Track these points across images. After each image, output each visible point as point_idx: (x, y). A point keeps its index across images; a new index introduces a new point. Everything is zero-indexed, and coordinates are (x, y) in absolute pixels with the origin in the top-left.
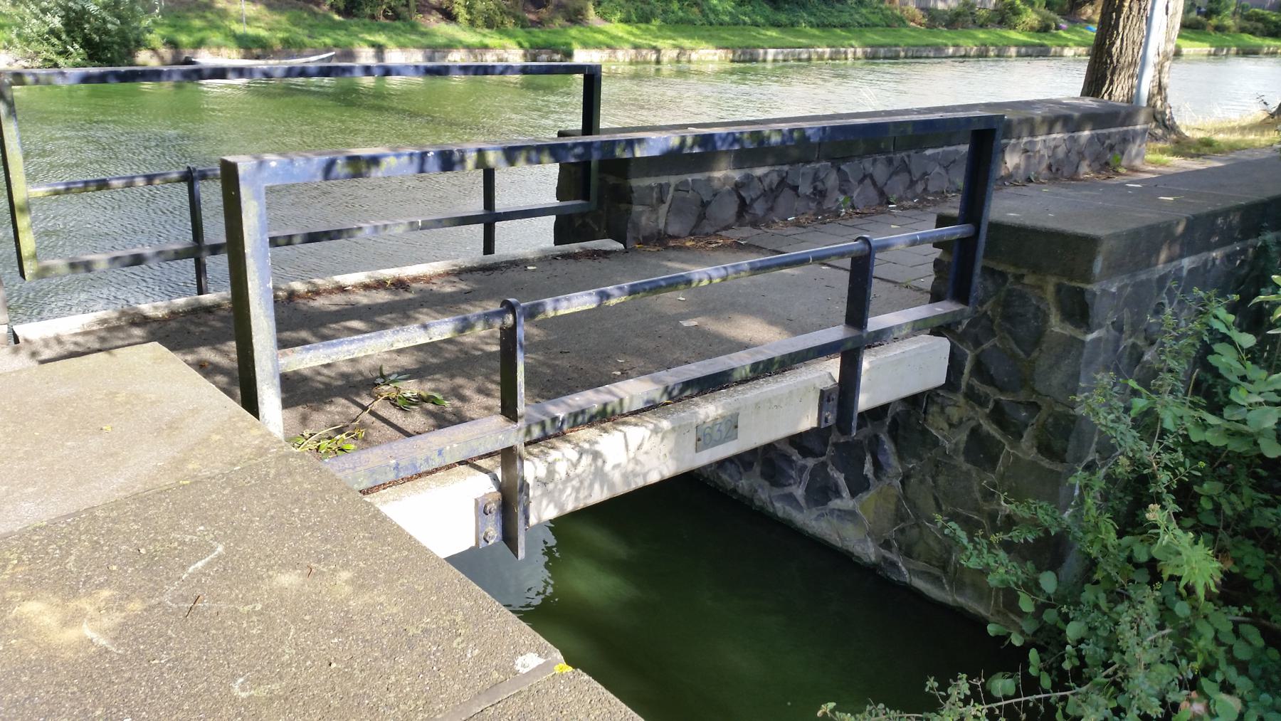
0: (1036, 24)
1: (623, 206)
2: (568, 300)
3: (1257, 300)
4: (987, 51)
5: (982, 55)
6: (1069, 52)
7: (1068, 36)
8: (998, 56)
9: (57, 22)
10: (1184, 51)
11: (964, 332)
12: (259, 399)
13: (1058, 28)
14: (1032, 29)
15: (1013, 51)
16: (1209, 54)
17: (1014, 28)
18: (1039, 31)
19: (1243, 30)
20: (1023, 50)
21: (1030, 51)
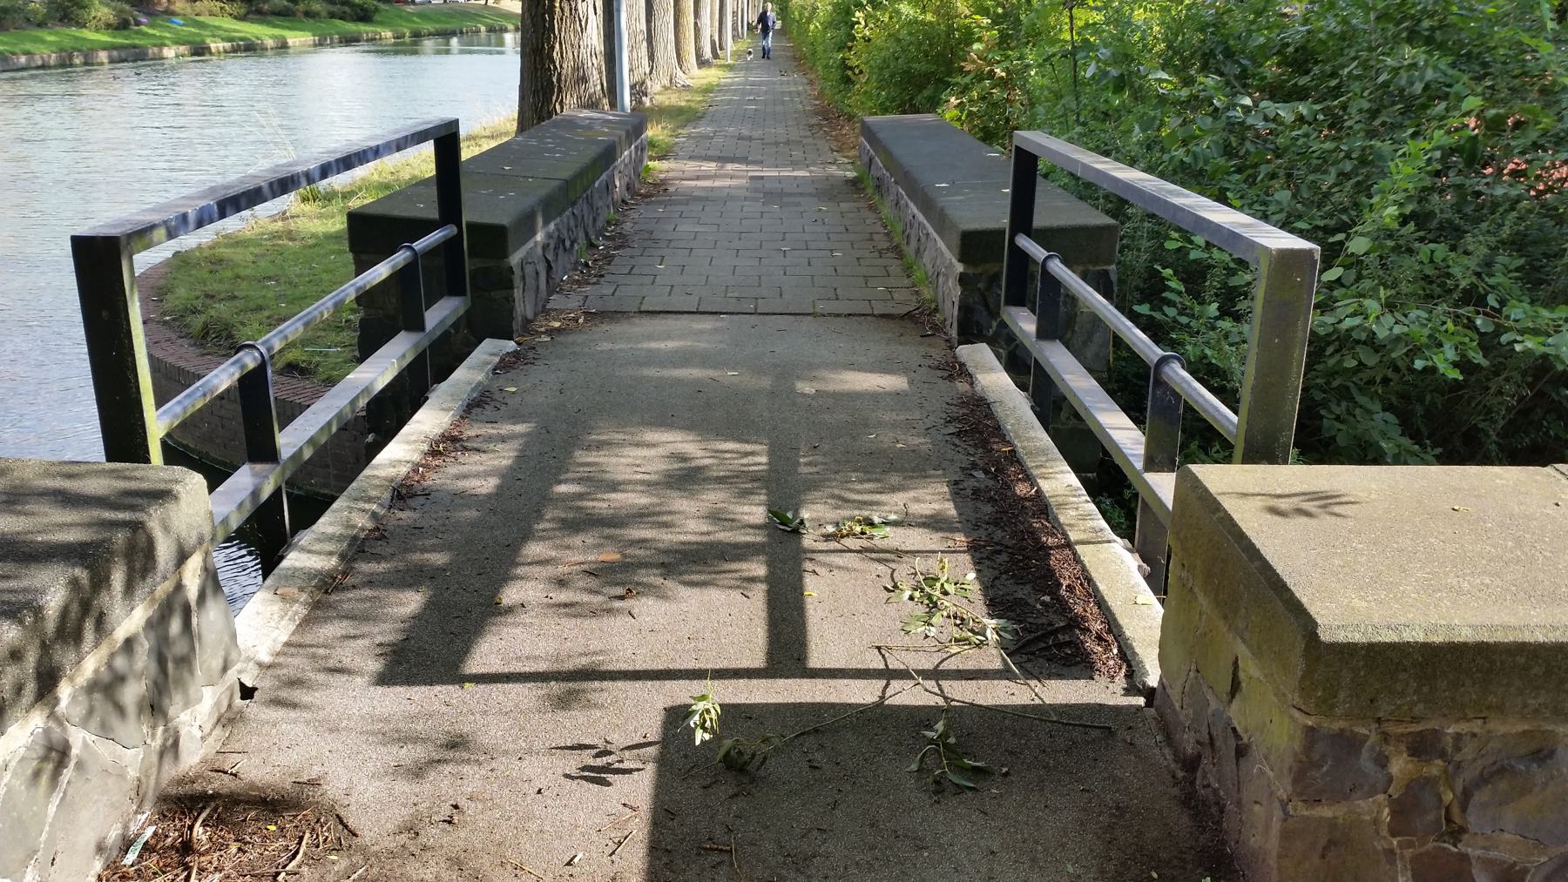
0: (112, 19)
1: (498, 295)
2: (176, 416)
3: (381, 271)
4: (71, 57)
5: (65, 63)
6: (169, 52)
7: (151, 31)
8: (86, 64)
9: (1452, 19)
10: (290, 42)
11: (995, 333)
12: (1389, 637)
13: (138, 23)
14: (108, 26)
15: (103, 56)
16: (315, 45)
17: (82, 25)
18: (117, 28)
19: (332, 15)
20: (115, 53)
21: (123, 55)
